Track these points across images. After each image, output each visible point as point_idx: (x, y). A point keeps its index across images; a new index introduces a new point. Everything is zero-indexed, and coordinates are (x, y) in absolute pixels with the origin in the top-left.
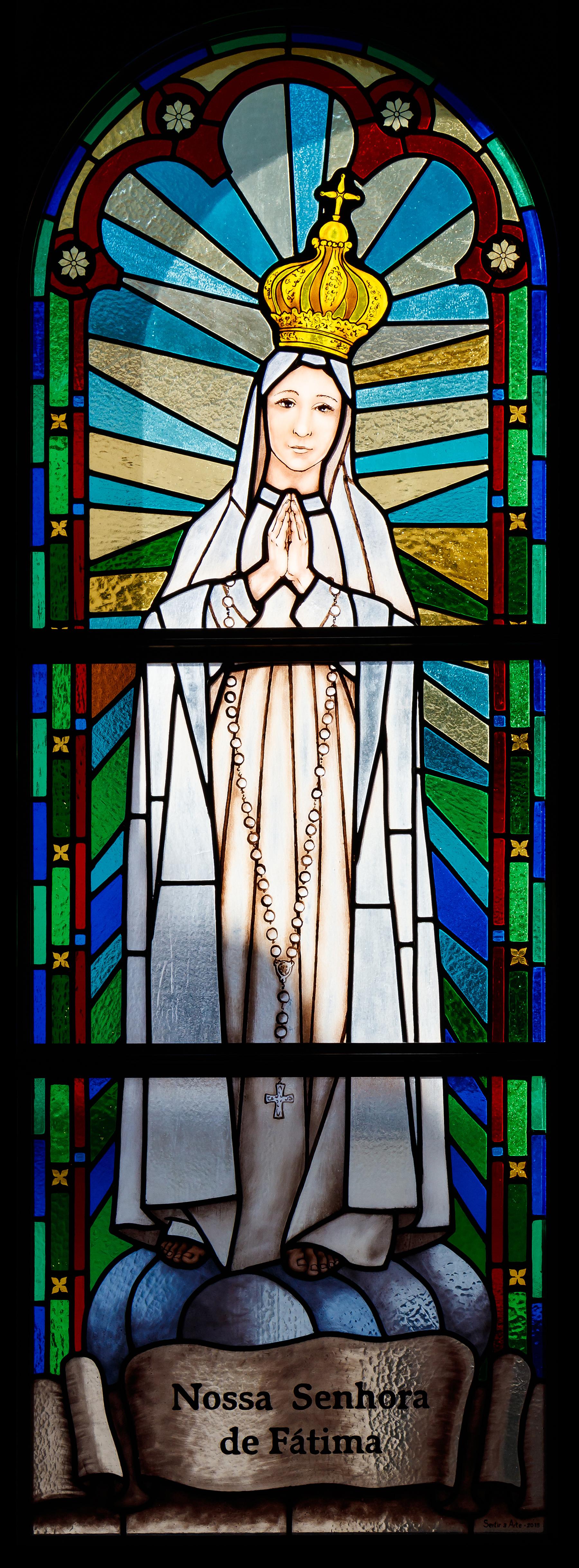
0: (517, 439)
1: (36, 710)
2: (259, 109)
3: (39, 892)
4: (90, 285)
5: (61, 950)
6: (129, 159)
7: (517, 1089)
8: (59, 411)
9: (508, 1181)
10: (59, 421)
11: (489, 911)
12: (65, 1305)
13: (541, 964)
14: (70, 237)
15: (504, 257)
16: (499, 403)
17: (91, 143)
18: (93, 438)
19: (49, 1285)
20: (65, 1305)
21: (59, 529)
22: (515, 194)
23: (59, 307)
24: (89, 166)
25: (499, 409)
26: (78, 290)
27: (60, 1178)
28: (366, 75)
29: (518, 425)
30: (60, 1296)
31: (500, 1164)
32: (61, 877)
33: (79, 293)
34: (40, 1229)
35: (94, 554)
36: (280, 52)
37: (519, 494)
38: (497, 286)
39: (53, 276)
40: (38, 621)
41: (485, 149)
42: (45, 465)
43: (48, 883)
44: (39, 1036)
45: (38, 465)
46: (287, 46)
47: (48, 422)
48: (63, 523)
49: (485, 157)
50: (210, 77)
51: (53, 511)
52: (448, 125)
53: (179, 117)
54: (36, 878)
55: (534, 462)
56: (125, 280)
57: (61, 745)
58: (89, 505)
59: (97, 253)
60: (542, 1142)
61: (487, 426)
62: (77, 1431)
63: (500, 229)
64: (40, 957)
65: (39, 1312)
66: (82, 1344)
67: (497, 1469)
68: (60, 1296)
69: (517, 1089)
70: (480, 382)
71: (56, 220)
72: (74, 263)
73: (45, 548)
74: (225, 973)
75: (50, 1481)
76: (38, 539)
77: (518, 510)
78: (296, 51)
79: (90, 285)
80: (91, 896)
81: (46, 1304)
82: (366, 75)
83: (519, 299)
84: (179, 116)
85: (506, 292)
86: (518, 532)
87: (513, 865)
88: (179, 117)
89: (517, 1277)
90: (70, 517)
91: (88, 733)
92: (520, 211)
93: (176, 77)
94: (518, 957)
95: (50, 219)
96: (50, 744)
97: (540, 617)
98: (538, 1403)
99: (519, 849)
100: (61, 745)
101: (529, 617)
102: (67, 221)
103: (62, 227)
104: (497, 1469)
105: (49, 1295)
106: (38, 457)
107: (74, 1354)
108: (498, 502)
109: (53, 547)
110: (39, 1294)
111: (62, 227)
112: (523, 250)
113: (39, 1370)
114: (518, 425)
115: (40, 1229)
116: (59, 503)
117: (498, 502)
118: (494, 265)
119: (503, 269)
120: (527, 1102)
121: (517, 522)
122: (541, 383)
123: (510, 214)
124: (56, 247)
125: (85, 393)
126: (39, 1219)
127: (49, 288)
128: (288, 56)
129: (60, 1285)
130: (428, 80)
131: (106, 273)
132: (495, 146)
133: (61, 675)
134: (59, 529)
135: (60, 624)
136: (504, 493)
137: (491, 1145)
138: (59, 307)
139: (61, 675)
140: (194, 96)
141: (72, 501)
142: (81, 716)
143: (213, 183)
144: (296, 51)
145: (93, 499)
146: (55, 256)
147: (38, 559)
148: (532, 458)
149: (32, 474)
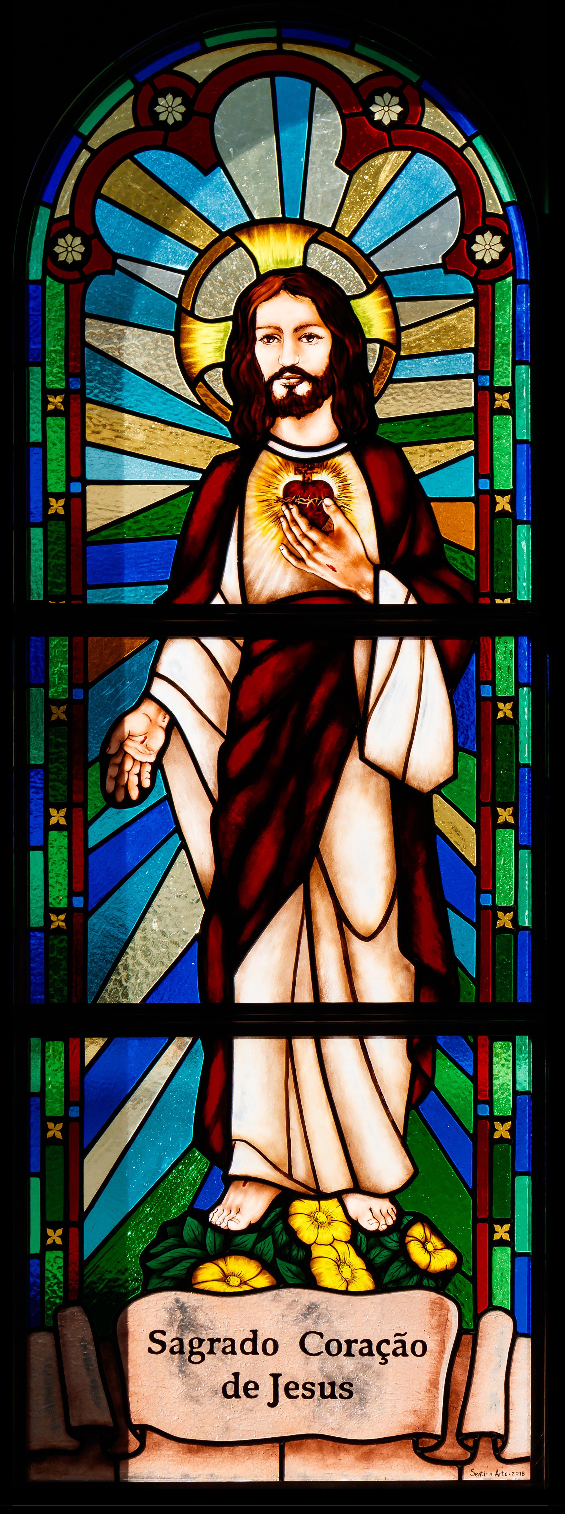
0: (502, 426)
1: (33, 843)
2: (252, 97)
3: (36, 858)
4: (86, 270)
6: (122, 149)
7: (502, 1051)
8: (56, 392)
11: (476, 870)
13: (527, 928)
16: (484, 388)
17: (86, 134)
19: (44, 1236)
21: (57, 506)
22: (498, 191)
23: (55, 290)
24: (84, 156)
25: (485, 394)
26: (76, 275)
27: (55, 1131)
28: (356, 71)
30: (56, 413)
31: (485, 1123)
32: (58, 841)
33: (76, 278)
34: (35, 1183)
35: (90, 526)
36: (273, 46)
37: (504, 478)
39: (49, 262)
40: (37, 591)
42: (43, 445)
43: (44, 848)
45: (36, 444)
46: (279, 40)
47: (45, 402)
52: (435, 119)
53: (170, 109)
55: (518, 446)
56: (120, 262)
57: (59, 713)
58: (86, 483)
59: (92, 238)
60: (525, 1102)
61: (472, 405)
63: (483, 222)
64: (36, 918)
65: (34, 1263)
67: (483, 1417)
69: (502, 1051)
70: (467, 363)
71: (53, 207)
73: (43, 525)
76: (37, 516)
77: (503, 493)
78: (287, 47)
79: (86, 270)
80: (83, 1264)
81: (41, 1256)
82: (356, 71)
84: (170, 109)
86: (503, 513)
90: (66, 495)
92: (504, 205)
93: (169, 70)
94: (505, 920)
95: (46, 205)
96: (48, 713)
97: (524, 593)
99: (505, 815)
100: (59, 713)
101: (513, 595)
102: (63, 208)
103: (57, 215)
104: (483, 1417)
105: (45, 1248)
106: (35, 436)
108: (484, 484)
110: (35, 1247)
111: (57, 215)
112: (507, 241)
114: (502, 411)
115: (35, 1183)
116: (56, 482)
117: (484, 484)
118: (478, 257)
119: (487, 260)
120: (512, 1069)
121: (503, 503)
122: (524, 372)
123: (494, 206)
125: (81, 376)
126: (35, 1175)
127: (46, 271)
128: (280, 51)
129: (55, 1236)
130: (414, 78)
131: (101, 258)
132: (478, 142)
133: (58, 646)
134: (57, 506)
135: (58, 598)
136: (491, 477)
138: (55, 290)
139: (58, 646)
140: (185, 88)
141: (69, 480)
143: (206, 170)
144: (287, 47)
145: (89, 476)
147: (36, 535)
148: (516, 442)
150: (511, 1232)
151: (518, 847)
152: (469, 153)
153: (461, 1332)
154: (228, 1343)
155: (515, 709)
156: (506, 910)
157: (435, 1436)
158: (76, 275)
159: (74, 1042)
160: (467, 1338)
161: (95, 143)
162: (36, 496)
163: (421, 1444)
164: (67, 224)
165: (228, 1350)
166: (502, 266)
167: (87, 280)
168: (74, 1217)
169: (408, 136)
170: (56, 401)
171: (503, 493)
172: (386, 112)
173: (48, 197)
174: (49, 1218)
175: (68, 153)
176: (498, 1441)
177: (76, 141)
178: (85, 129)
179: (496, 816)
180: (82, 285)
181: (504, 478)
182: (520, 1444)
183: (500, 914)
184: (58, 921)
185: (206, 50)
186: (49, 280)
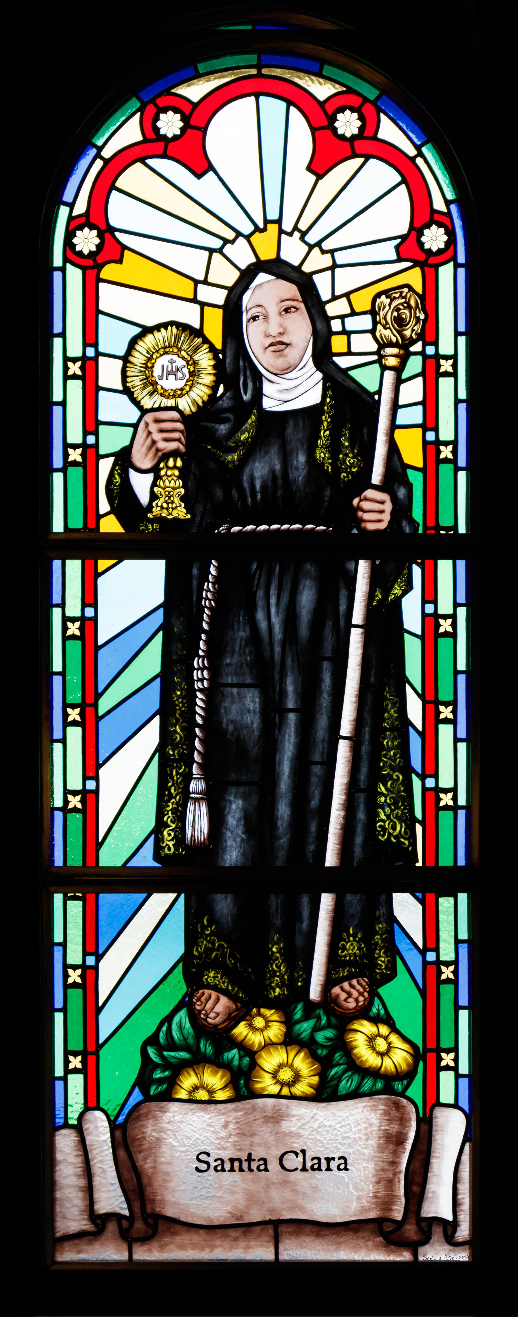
0: (446, 385)
4: (100, 259)
5: (75, 793)
10: (75, 368)
12: (80, 1078)
15: (434, 238)
18: (102, 285)
20: (80, 1078)
26: (90, 263)
28: (322, 90)
29: (446, 374)
30: (76, 1071)
33: (92, 266)
36: (254, 71)
41: (420, 154)
43: (63, 741)
48: (78, 624)
49: (419, 161)
50: (194, 91)
62: (88, 1202)
64: (58, 802)
65: (59, 1085)
66: (92, 1102)
68: (76, 1071)
69: (445, 903)
71: (72, 206)
73: (64, 470)
74: (194, 1229)
75: (70, 1216)
76: (58, 462)
77: (446, 444)
78: (265, 71)
79: (100, 259)
81: (65, 1079)
82: (322, 90)
83: (446, 272)
85: (436, 267)
88: (170, 124)
89: (447, 1059)
91: (96, 968)
92: (448, 203)
98: (466, 1158)
105: (67, 1071)
106: (57, 396)
107: (87, 1108)
110: (59, 1071)
111: (75, 213)
113: (60, 1121)
114: (446, 374)
123: (439, 205)
127: (66, 260)
128: (260, 75)
129: (76, 1062)
138: (74, 275)
141: (85, 954)
142: (90, 954)
144: (265, 71)
150: (456, 1060)
151: (456, 740)
154: (219, 1162)
155: (454, 625)
158: (90, 263)
161: (107, 153)
163: (380, 1228)
164: (83, 220)
165: (219, 1168)
166: (447, 253)
168: (91, 1048)
169: (366, 145)
172: (347, 124)
174: (70, 1048)
179: (438, 713)
181: (446, 432)
182: (464, 1231)
184: (75, 801)
185: (198, 76)
186: (68, 265)
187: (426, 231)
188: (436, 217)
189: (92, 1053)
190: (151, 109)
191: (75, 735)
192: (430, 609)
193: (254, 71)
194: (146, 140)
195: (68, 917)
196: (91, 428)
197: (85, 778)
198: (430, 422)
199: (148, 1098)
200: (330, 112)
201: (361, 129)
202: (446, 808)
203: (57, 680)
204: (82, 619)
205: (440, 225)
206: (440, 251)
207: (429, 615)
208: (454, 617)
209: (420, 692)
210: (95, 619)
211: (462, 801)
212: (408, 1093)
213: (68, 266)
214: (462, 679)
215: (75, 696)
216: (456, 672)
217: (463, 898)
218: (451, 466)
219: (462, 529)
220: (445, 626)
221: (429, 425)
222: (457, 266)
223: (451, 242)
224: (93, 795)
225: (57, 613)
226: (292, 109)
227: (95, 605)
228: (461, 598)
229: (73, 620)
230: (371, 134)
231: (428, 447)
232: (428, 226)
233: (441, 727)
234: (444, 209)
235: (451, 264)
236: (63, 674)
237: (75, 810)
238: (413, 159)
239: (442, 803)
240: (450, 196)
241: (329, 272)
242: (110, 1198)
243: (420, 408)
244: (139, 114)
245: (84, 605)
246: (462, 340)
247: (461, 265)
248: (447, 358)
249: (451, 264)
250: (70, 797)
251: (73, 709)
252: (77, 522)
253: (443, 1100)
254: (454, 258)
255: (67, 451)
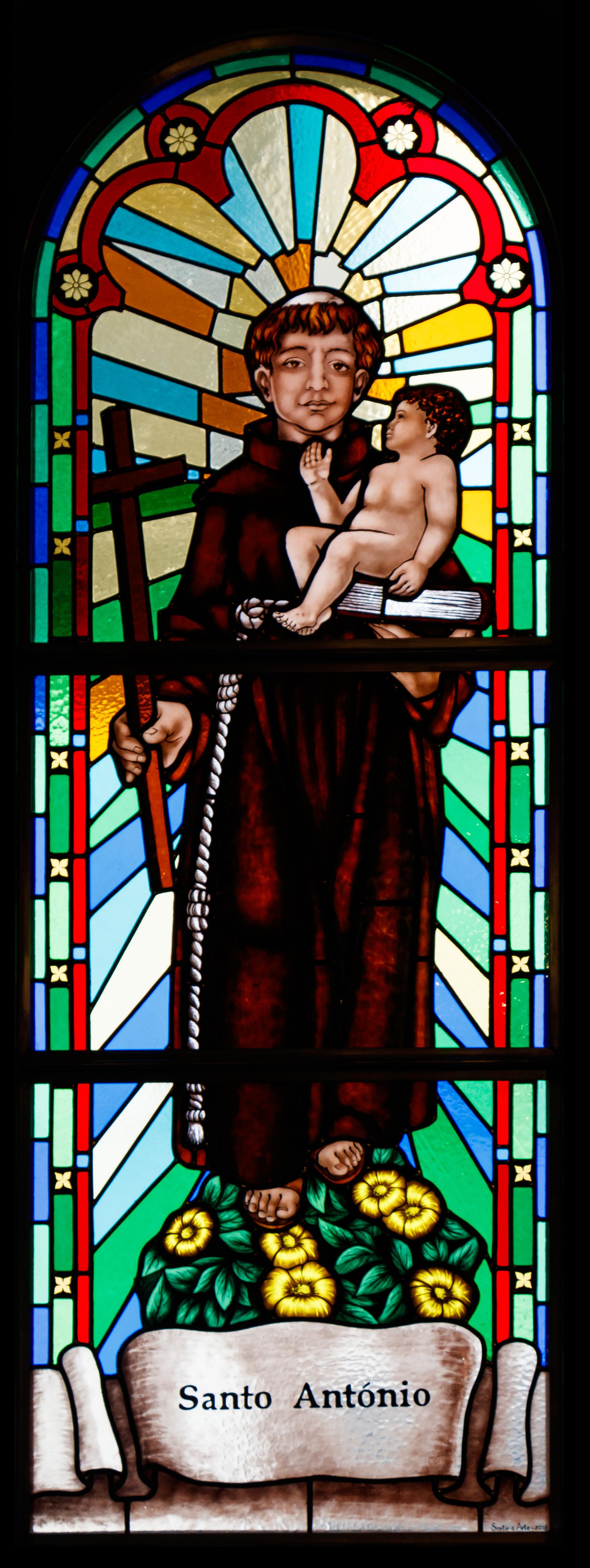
0: (520, 456)
1: (37, 1217)
4: (93, 308)
6: (134, 178)
8: (62, 430)
9: (510, 763)
14: (74, 259)
15: (507, 276)
23: (62, 327)
24: (92, 188)
26: (81, 311)
28: (369, 99)
29: (520, 869)
36: (286, 75)
37: (522, 1148)
38: (501, 307)
40: (41, 636)
42: (49, 486)
43: (46, 897)
44: (40, 1045)
47: (52, 440)
51: (56, 529)
53: (182, 140)
54: (37, 561)
59: (99, 275)
65: (40, 328)
66: (83, 1336)
71: (58, 241)
72: (76, 285)
73: (48, 566)
75: (52, 1470)
76: (41, 556)
77: (522, 527)
78: (299, 74)
79: (93, 308)
82: (369, 99)
83: (522, 318)
84: (182, 139)
85: (511, 311)
87: (516, 555)
88: (182, 140)
92: (524, 231)
95: (51, 240)
102: (70, 241)
103: (64, 248)
105: (52, 1296)
106: (40, 476)
109: (56, 563)
111: (64, 248)
121: (522, 538)
123: (513, 234)
124: (58, 269)
127: (51, 309)
132: (497, 168)
134: (63, 547)
136: (508, 510)
137: (493, 937)
138: (62, 327)
140: (197, 119)
144: (299, 74)
146: (56, 281)
147: (41, 575)
149: (34, 495)
151: (534, 889)
152: (489, 182)
153: (485, 1363)
156: (521, 954)
157: (452, 1478)
158: (81, 311)
159: (83, 1087)
160: (488, 1372)
161: (103, 175)
162: (40, 538)
166: (522, 295)
167: (94, 317)
170: (62, 440)
171: (522, 527)
173: (53, 232)
175: (70, 191)
176: (515, 1483)
177: (81, 174)
178: (91, 161)
180: (89, 320)
181: (521, 513)
183: (515, 959)
187: (496, 267)
188: (509, 249)
189: (79, 856)
190: (158, 122)
191: (60, 893)
192: (502, 518)
193: (286, 75)
194: (151, 160)
195: (52, 1110)
196: (82, 406)
197: (76, 1152)
198: (501, 500)
199: (151, 1323)
200: (379, 124)
201: (417, 143)
202: (521, 974)
203: (40, 824)
204: (70, 962)
205: (513, 259)
206: (514, 292)
207: (502, 526)
208: (530, 740)
209: (487, 1033)
210: (86, 962)
211: (540, 964)
212: (472, 1322)
213: (55, 317)
214: (540, 815)
215: (61, 844)
216: (534, 808)
217: (542, 1085)
218: (528, 555)
219: (542, 631)
220: (519, 751)
221: (499, 399)
222: (535, 310)
223: (528, 281)
224: (83, 753)
225: (40, 742)
226: (331, 119)
227: (86, 945)
228: (540, 718)
229: (59, 750)
230: (429, 151)
231: (496, 958)
232: (499, 261)
233: (514, 877)
234: (519, 238)
235: (528, 308)
236: (46, 815)
237: (59, 984)
238: (480, 180)
239: (517, 544)
240: (527, 222)
241: (377, 303)
242: (104, 1453)
243: (489, 344)
244: (143, 128)
245: (73, 945)
246: (542, 400)
247: (541, 309)
248: (522, 422)
249: (528, 308)
250: (54, 969)
251: (59, 980)
252: (63, 631)
253: (517, 1334)
254: (532, 301)
255: (53, 435)
